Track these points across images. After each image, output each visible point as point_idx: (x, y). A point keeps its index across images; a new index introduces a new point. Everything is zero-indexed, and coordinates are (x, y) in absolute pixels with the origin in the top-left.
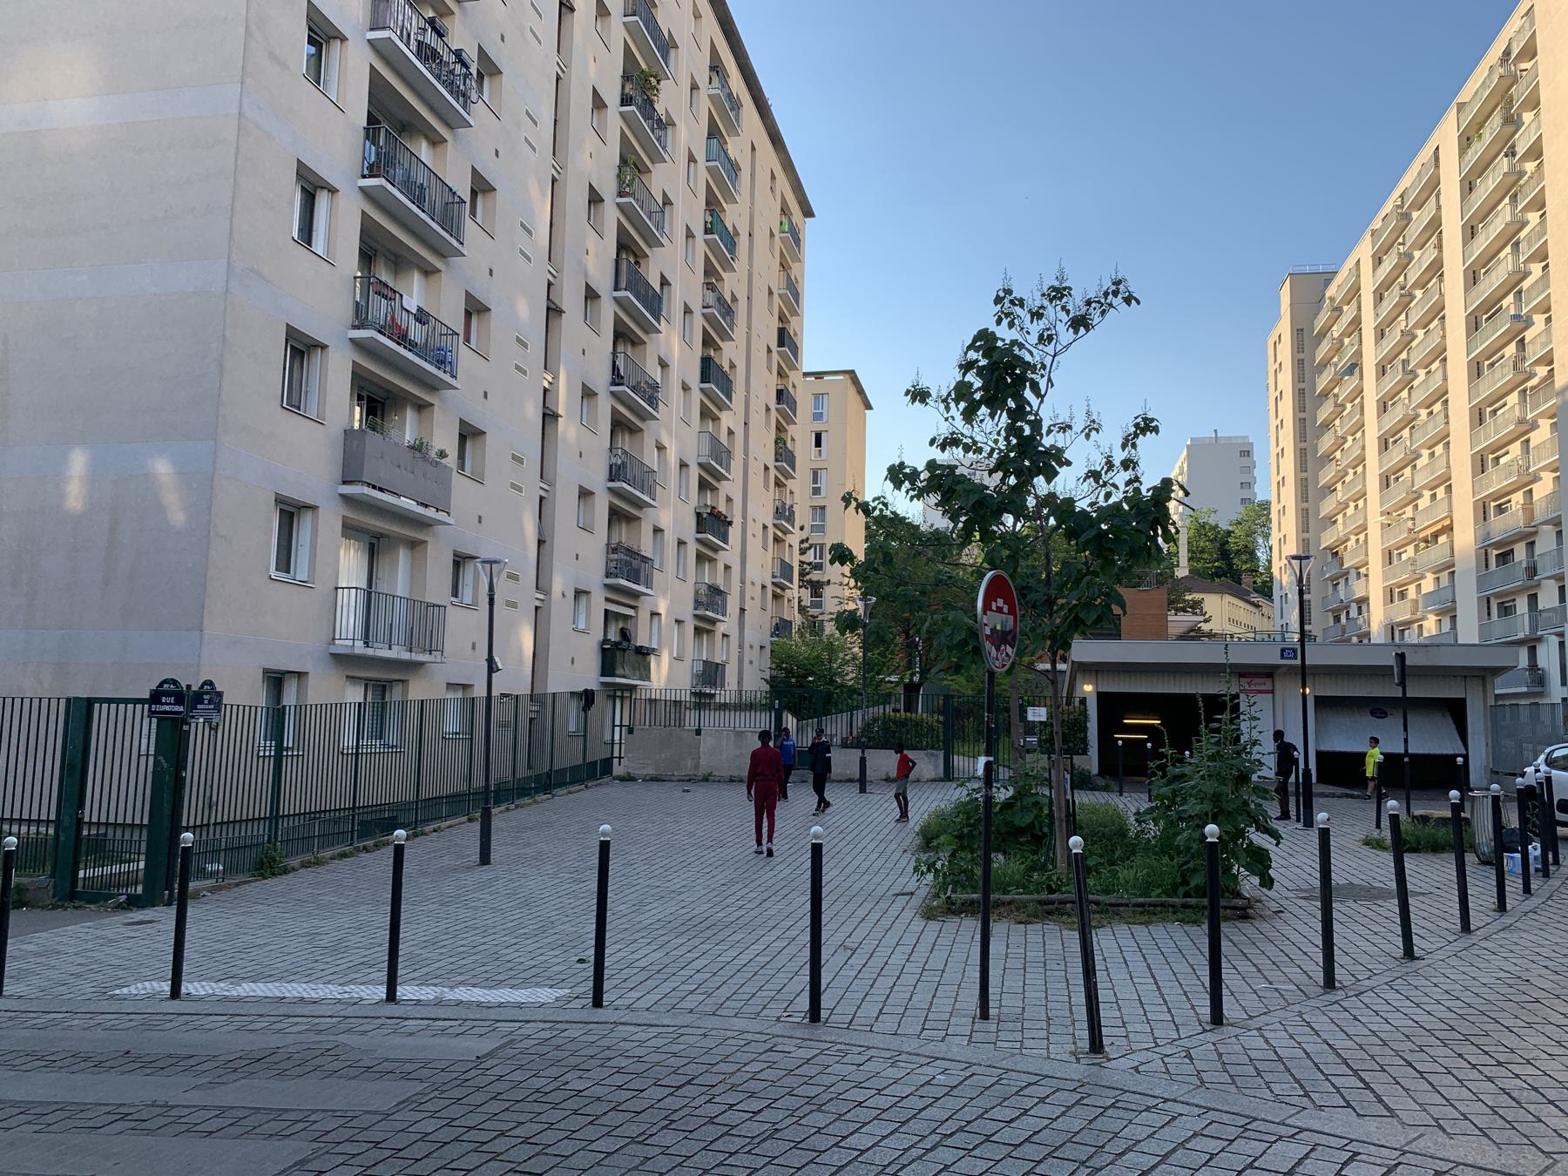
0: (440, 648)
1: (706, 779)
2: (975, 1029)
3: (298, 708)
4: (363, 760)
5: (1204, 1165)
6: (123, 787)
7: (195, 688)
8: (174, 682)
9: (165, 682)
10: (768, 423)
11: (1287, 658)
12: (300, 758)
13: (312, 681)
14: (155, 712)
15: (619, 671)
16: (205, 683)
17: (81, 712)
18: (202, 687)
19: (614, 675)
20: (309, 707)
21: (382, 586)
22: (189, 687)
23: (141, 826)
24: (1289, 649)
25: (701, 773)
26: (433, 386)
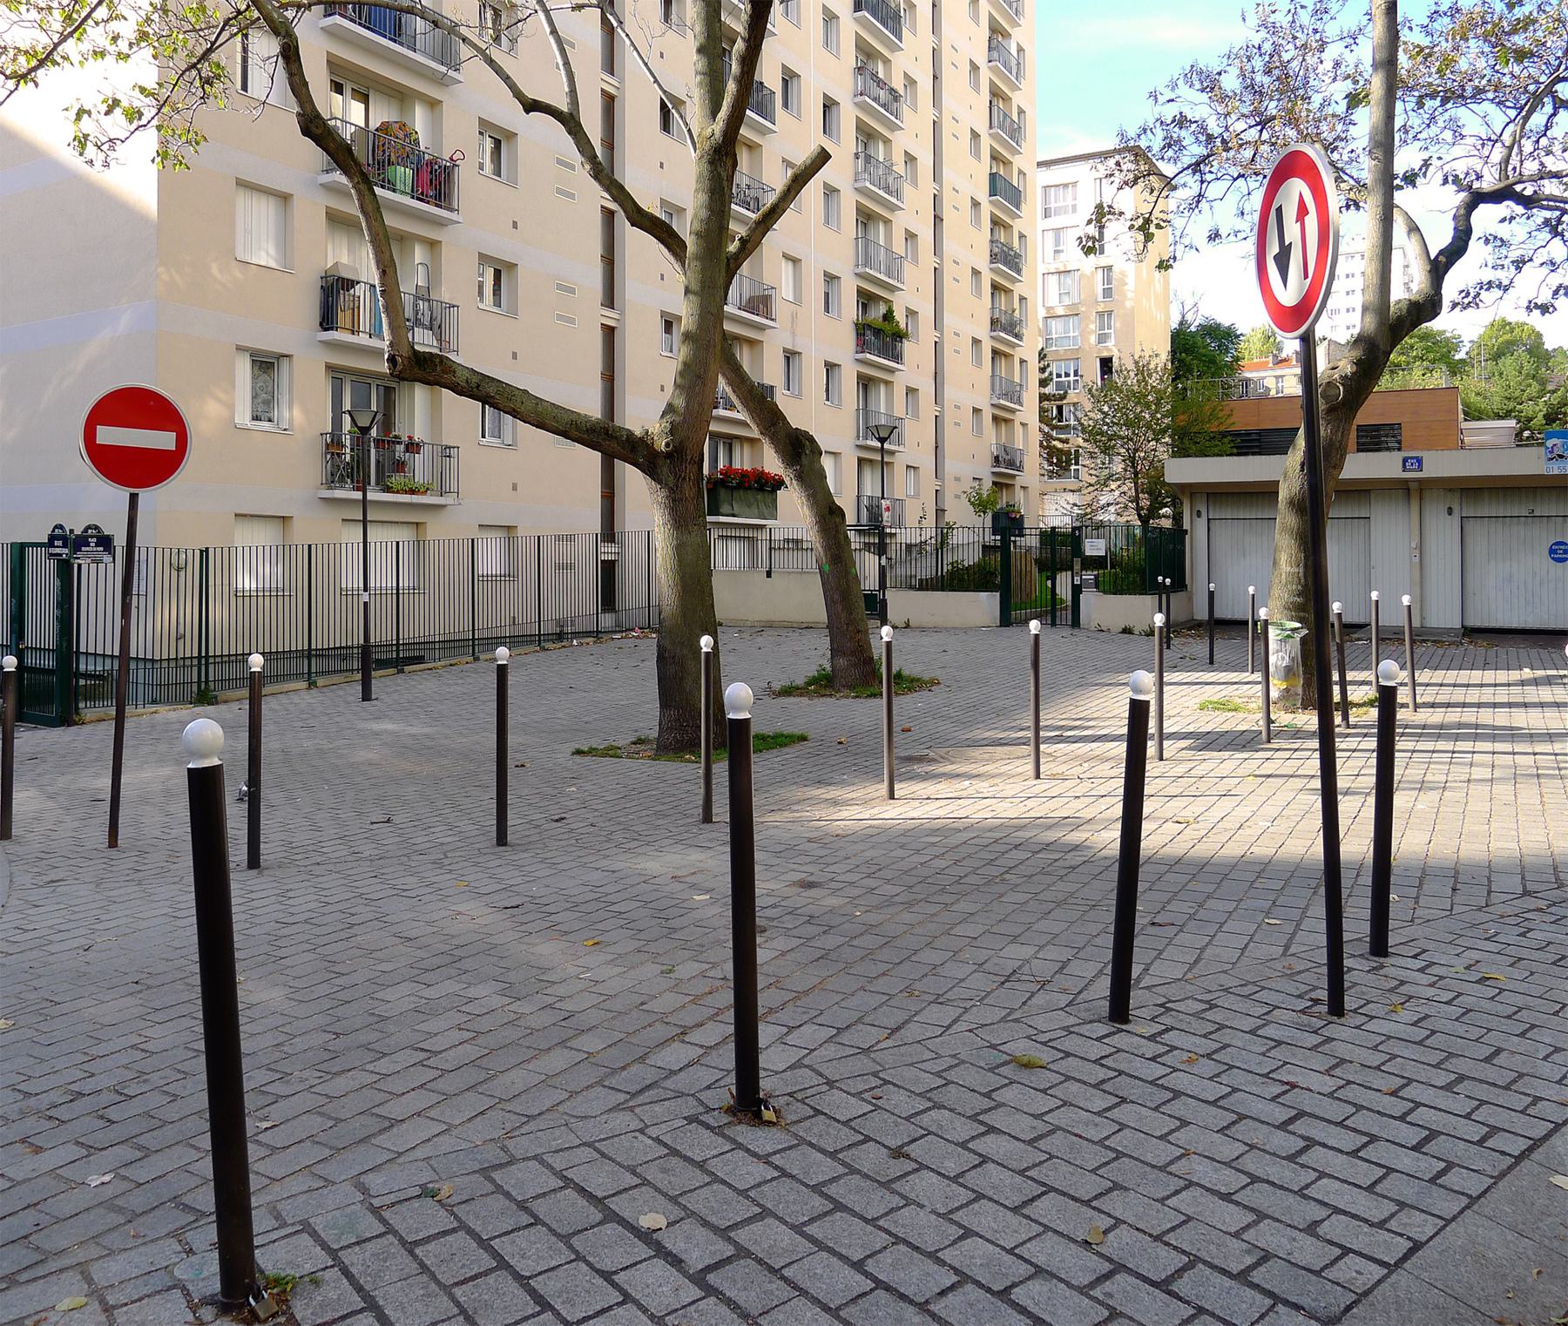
0: (454, 488)
1: (560, 636)
2: (1378, 1272)
3: (287, 548)
4: (404, 600)
5: (19, 1183)
6: (287, 628)
7: (78, 532)
8: (96, 527)
9: (89, 527)
10: (977, 221)
11: (1410, 470)
12: (287, 599)
13: (297, 524)
14: (52, 555)
15: (725, 508)
16: (56, 527)
17: (19, 552)
18: (86, 530)
19: (718, 514)
20: (344, 546)
21: (872, 407)
22: (72, 531)
23: (112, 657)
24: (1412, 458)
25: (549, 628)
26: (893, 208)
